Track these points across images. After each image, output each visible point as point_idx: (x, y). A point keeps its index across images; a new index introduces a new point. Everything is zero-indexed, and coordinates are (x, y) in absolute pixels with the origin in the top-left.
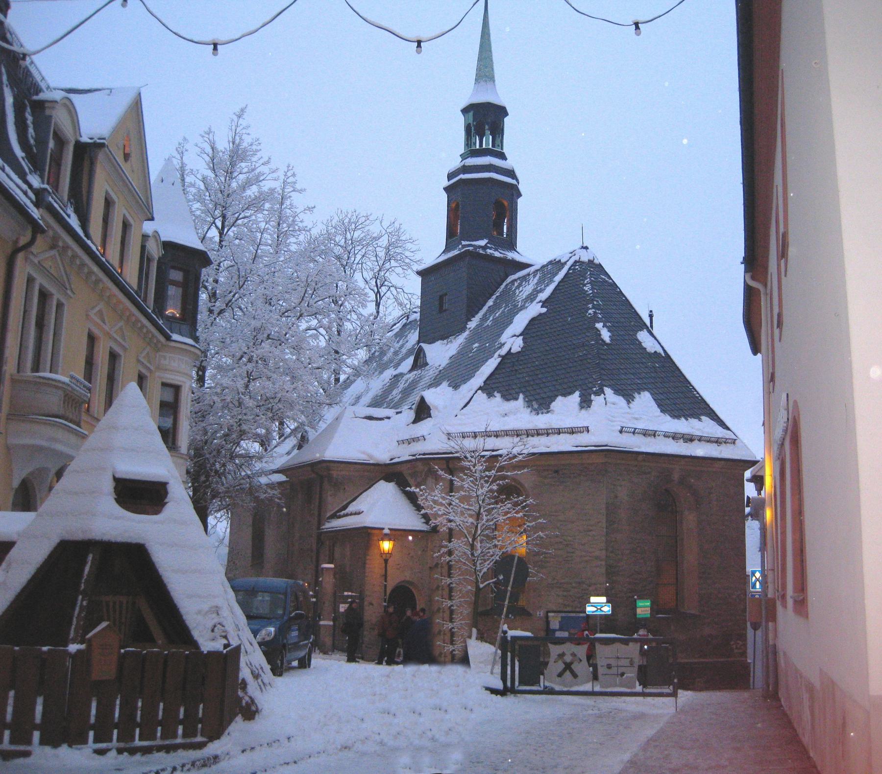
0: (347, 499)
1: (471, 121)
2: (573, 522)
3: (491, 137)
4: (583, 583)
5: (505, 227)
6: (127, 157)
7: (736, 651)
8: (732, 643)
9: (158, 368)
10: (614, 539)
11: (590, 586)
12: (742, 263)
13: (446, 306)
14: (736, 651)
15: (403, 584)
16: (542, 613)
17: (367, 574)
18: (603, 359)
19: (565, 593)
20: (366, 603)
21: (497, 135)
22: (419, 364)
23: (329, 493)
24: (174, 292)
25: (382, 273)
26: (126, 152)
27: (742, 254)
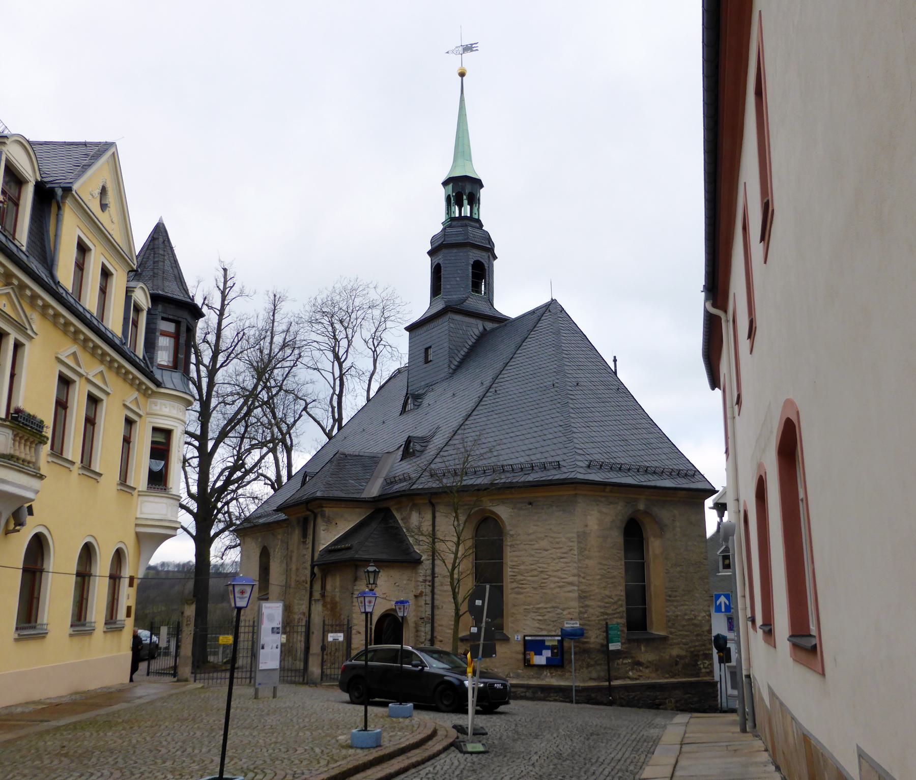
1: (450, 192)
2: (547, 550)
3: (469, 207)
4: (557, 607)
5: (483, 286)
6: (104, 207)
7: (704, 670)
8: (699, 663)
9: (149, 414)
10: (585, 566)
11: (563, 610)
12: (702, 291)
13: (430, 358)
14: (704, 670)
15: (387, 612)
16: (519, 637)
18: (572, 399)
19: (540, 618)
20: (354, 632)
21: (474, 205)
22: (407, 410)
23: (322, 528)
24: (164, 342)
25: (378, 334)
26: (103, 202)
27: (702, 282)
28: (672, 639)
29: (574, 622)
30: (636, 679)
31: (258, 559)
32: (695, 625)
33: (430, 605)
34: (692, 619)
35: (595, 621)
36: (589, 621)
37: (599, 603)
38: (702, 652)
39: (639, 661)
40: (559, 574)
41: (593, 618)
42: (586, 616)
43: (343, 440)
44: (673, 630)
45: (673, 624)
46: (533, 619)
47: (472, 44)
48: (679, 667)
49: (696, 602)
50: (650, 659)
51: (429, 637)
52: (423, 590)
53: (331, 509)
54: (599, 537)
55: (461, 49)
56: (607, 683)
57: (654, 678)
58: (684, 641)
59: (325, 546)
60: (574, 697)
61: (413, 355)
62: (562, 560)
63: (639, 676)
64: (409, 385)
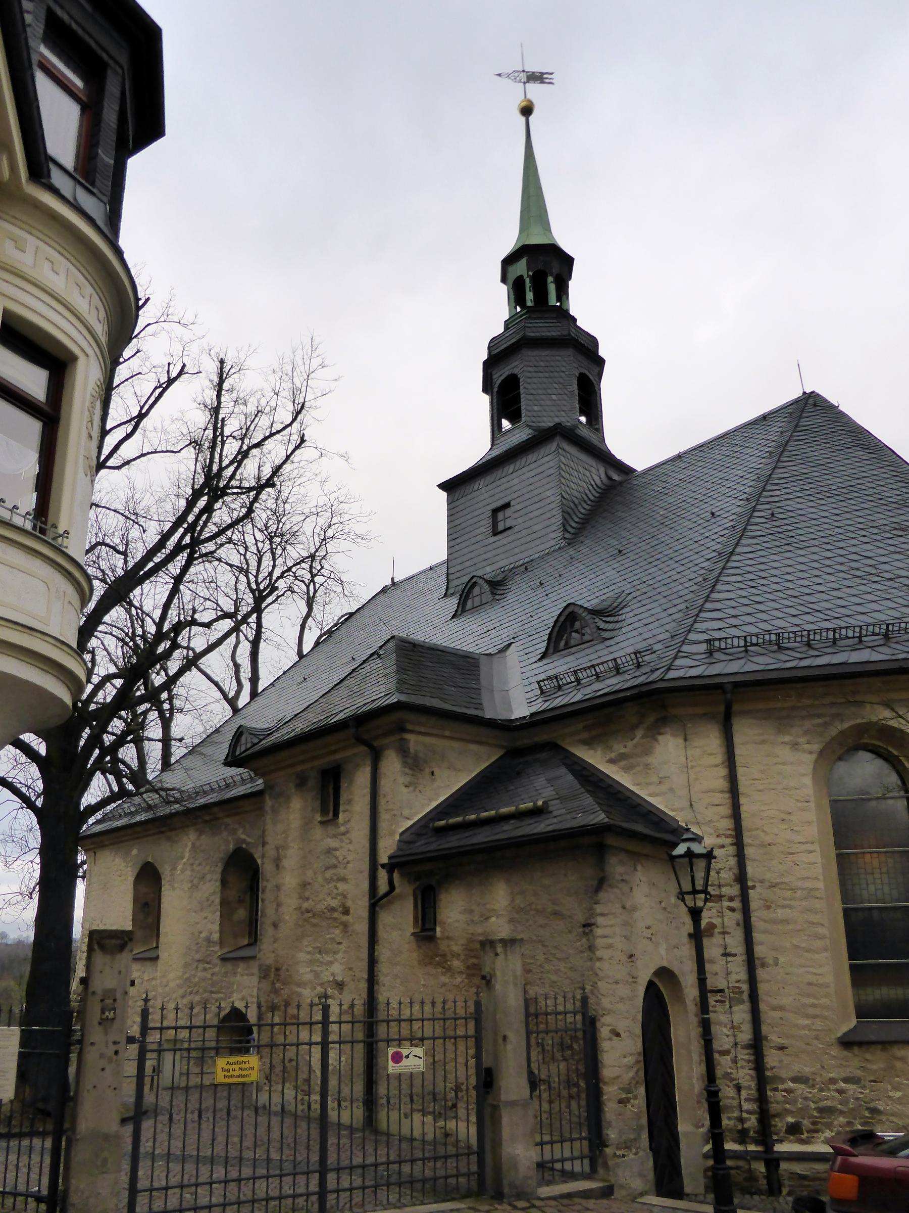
0: (438, 795)
17: (599, 953)
20: (604, 1032)
22: (467, 608)
31: (130, 886)
33: (741, 959)
43: (301, 683)
47: (543, 74)
51: (745, 1036)
52: (717, 921)
53: (421, 738)
55: (523, 76)
59: (410, 823)
61: (455, 536)
64: (451, 577)
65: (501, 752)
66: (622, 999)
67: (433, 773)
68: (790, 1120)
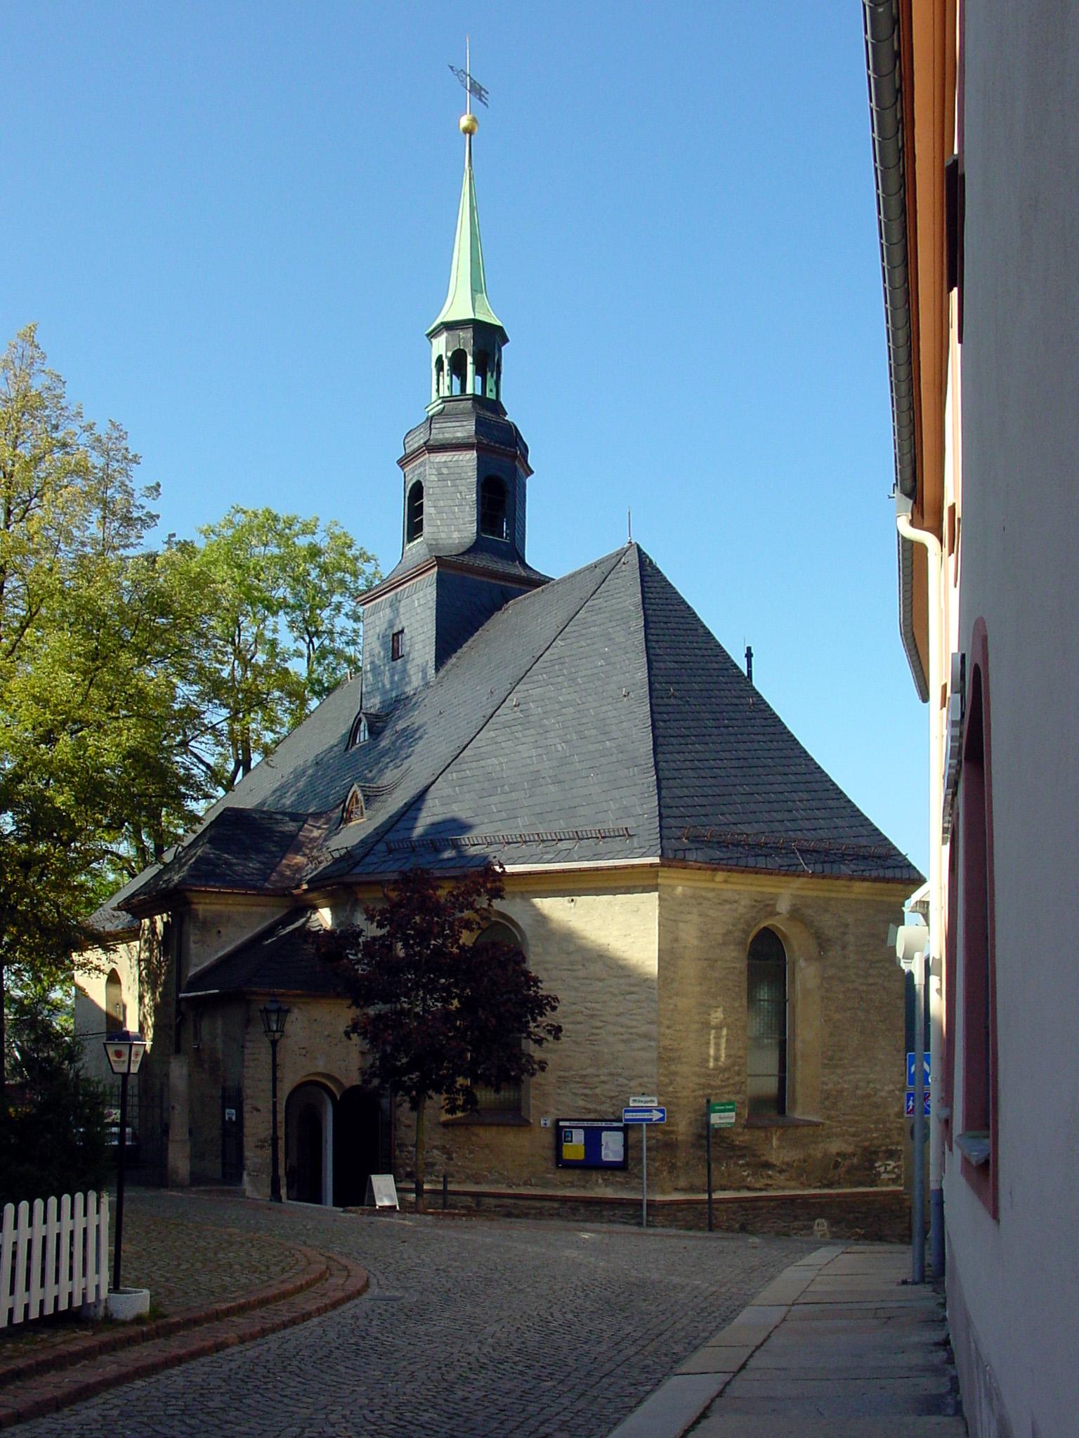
7: (884, 1176)
8: (877, 1165)
10: (671, 1007)
16: (549, 1123)
17: (246, 1064)
20: (246, 1108)
23: (192, 938)
27: (945, 1205)
28: (831, 1127)
29: (649, 1099)
30: (761, 1190)
32: (876, 1106)
34: (869, 1096)
35: (688, 1098)
36: (677, 1097)
37: (697, 1069)
38: (884, 1148)
39: (767, 1161)
40: (623, 1020)
41: (685, 1094)
42: (671, 1089)
44: (833, 1113)
45: (834, 1104)
46: (575, 1094)
48: (842, 1170)
49: (878, 1068)
50: (786, 1159)
53: (208, 907)
54: (699, 959)
56: (706, 1196)
57: (794, 1188)
58: (852, 1130)
60: (645, 1217)
62: (628, 997)
63: (767, 1185)
65: (285, 911)
66: (263, 1090)
67: (219, 932)
68: (409, 1169)
